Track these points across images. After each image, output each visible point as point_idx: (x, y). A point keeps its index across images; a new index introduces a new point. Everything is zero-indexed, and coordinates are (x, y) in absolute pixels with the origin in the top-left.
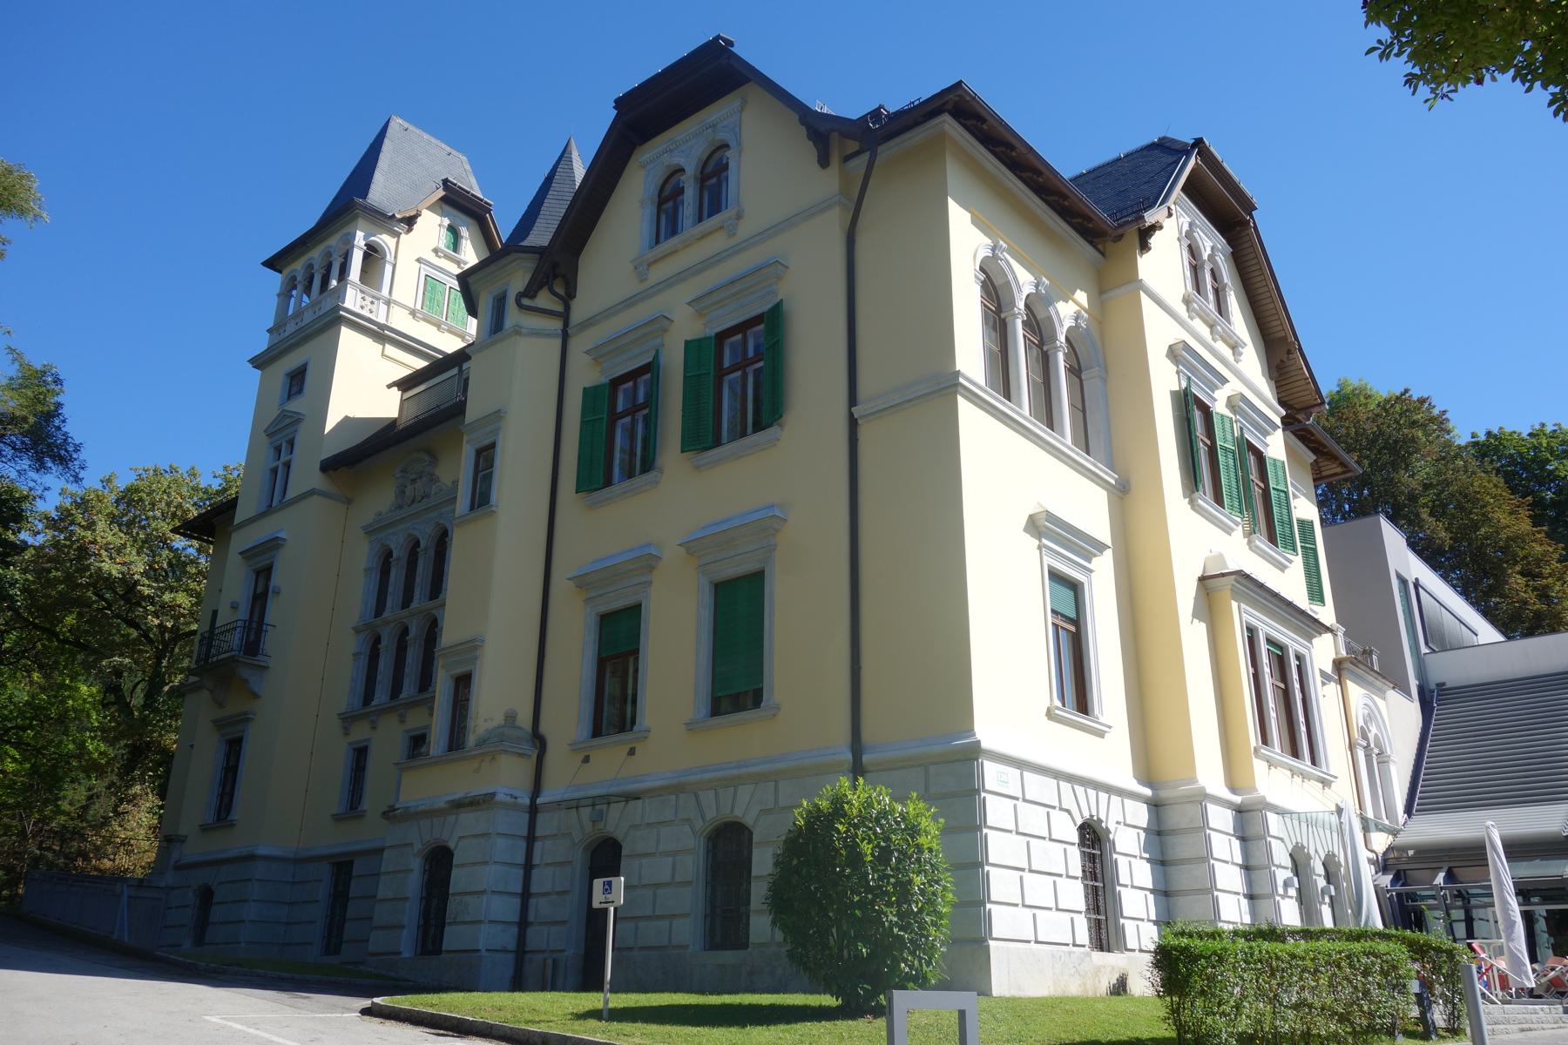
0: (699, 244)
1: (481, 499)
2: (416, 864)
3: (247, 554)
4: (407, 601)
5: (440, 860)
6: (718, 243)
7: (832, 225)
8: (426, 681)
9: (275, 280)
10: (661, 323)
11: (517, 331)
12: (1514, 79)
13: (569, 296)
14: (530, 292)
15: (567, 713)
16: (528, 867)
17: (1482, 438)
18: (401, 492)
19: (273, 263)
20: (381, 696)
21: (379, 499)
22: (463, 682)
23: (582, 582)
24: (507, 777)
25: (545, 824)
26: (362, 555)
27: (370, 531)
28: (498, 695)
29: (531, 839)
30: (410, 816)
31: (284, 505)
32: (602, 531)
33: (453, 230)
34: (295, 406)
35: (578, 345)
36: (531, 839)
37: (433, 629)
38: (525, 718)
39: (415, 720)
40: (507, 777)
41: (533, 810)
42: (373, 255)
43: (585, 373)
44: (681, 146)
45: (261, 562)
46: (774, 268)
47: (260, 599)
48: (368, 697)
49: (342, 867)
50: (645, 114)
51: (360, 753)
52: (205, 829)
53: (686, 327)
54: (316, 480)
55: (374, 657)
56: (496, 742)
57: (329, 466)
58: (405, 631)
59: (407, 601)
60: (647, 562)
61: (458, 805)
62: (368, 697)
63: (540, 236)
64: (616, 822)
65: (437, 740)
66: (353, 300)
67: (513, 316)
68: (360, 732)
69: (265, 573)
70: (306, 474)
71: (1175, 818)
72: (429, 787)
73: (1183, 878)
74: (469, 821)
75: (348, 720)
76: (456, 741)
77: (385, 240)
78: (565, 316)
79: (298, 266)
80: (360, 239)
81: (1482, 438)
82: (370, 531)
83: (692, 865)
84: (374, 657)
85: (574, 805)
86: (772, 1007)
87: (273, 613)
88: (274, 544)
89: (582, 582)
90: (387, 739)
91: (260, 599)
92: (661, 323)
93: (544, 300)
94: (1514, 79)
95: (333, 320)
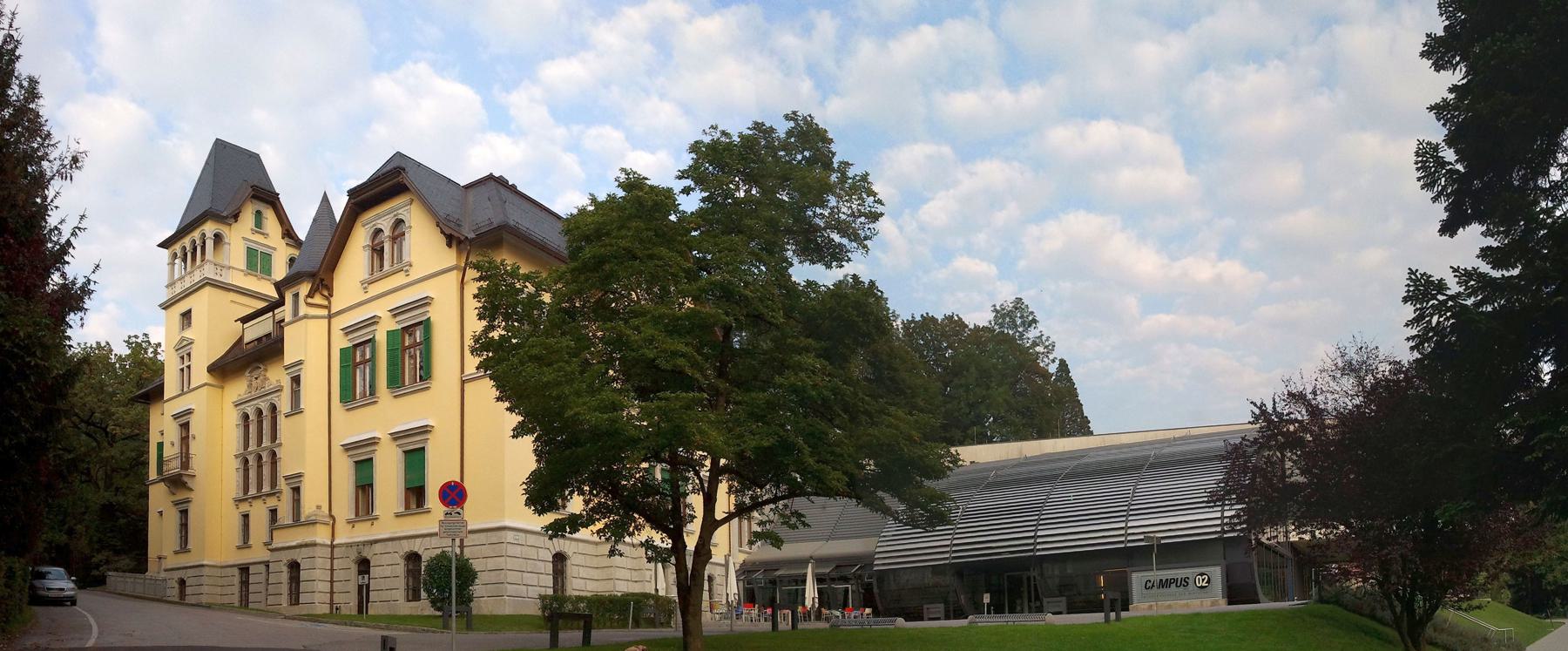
1: (296, 409)
2: (285, 569)
3: (176, 417)
5: (294, 567)
6: (399, 280)
8: (274, 483)
9: (165, 253)
10: (373, 321)
11: (306, 317)
13: (329, 297)
16: (332, 570)
17: (918, 318)
18: (250, 386)
19: (165, 245)
20: (253, 491)
21: (238, 389)
32: (357, 425)
39: (272, 502)
42: (218, 238)
43: (341, 342)
44: (381, 217)
45: (183, 420)
47: (185, 440)
48: (246, 489)
49: (244, 569)
50: (365, 198)
51: (246, 517)
52: (176, 553)
55: (246, 470)
58: (260, 457)
60: (373, 442)
62: (246, 489)
64: (367, 553)
65: (285, 516)
67: (303, 310)
68: (244, 507)
69: (185, 426)
75: (238, 501)
78: (328, 307)
79: (177, 247)
81: (918, 318)
83: (401, 569)
84: (246, 470)
85: (349, 545)
87: (194, 448)
88: (189, 412)
89: (348, 448)
91: (185, 440)
93: (318, 299)
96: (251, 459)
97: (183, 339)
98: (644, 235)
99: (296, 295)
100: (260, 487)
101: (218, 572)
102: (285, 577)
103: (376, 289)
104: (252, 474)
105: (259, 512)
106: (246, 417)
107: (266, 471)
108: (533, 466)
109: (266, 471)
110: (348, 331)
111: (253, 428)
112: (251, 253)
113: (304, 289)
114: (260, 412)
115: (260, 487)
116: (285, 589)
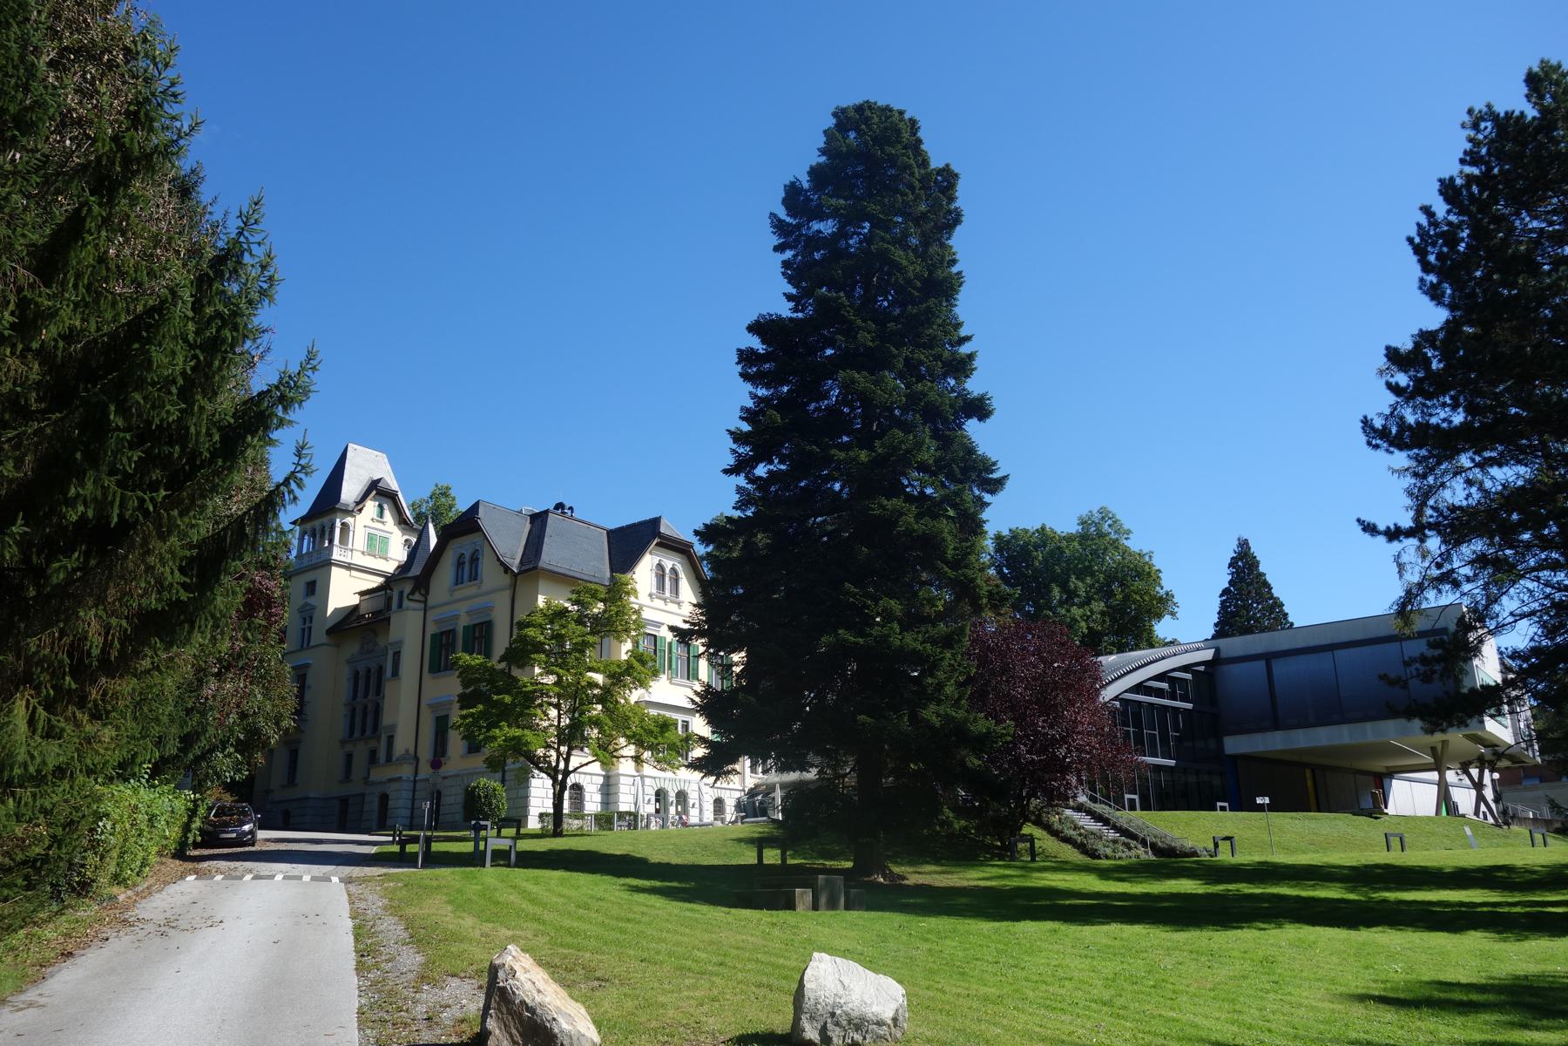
0: (469, 589)
1: (395, 673)
4: (366, 696)
5: (384, 799)
7: (507, 595)
12: (968, 339)
13: (427, 592)
14: (412, 593)
15: (426, 753)
20: (357, 734)
21: (352, 648)
22: (391, 739)
23: (431, 706)
24: (406, 771)
25: (419, 786)
26: (345, 673)
27: (348, 662)
28: (403, 743)
29: (414, 791)
30: (373, 783)
31: (309, 647)
33: (380, 506)
34: (312, 600)
35: (431, 616)
36: (414, 791)
37: (378, 710)
38: (412, 751)
39: (373, 744)
40: (406, 771)
41: (415, 781)
42: (345, 526)
46: (491, 609)
53: (464, 621)
54: (324, 639)
56: (403, 759)
57: (330, 632)
58: (366, 707)
59: (366, 696)
61: (391, 780)
63: (416, 570)
65: (382, 755)
66: (337, 554)
67: (406, 603)
68: (349, 748)
70: (318, 636)
71: (612, 781)
72: (378, 774)
73: (612, 799)
74: (395, 786)
75: (343, 743)
76: (389, 759)
77: (349, 520)
78: (425, 602)
79: (308, 526)
80: (338, 524)
82: (348, 662)
83: (460, 799)
86: (551, 852)
87: (307, 697)
88: (307, 666)
89: (431, 706)
90: (361, 752)
92: (457, 617)
93: (417, 596)
94: (968, 339)
95: (328, 564)
96: (359, 712)
97: (306, 604)
98: (399, 895)
99: (401, 593)
100: (363, 731)
101: (836, 943)
102: (376, 806)
103: (458, 595)
104: (358, 720)
105: (361, 752)
106: (357, 673)
107: (370, 718)
108: (956, 310)
109: (370, 718)
110: (437, 622)
111: (361, 684)
112: (371, 537)
113: (408, 588)
114: (369, 671)
115: (363, 731)
116: (375, 816)
